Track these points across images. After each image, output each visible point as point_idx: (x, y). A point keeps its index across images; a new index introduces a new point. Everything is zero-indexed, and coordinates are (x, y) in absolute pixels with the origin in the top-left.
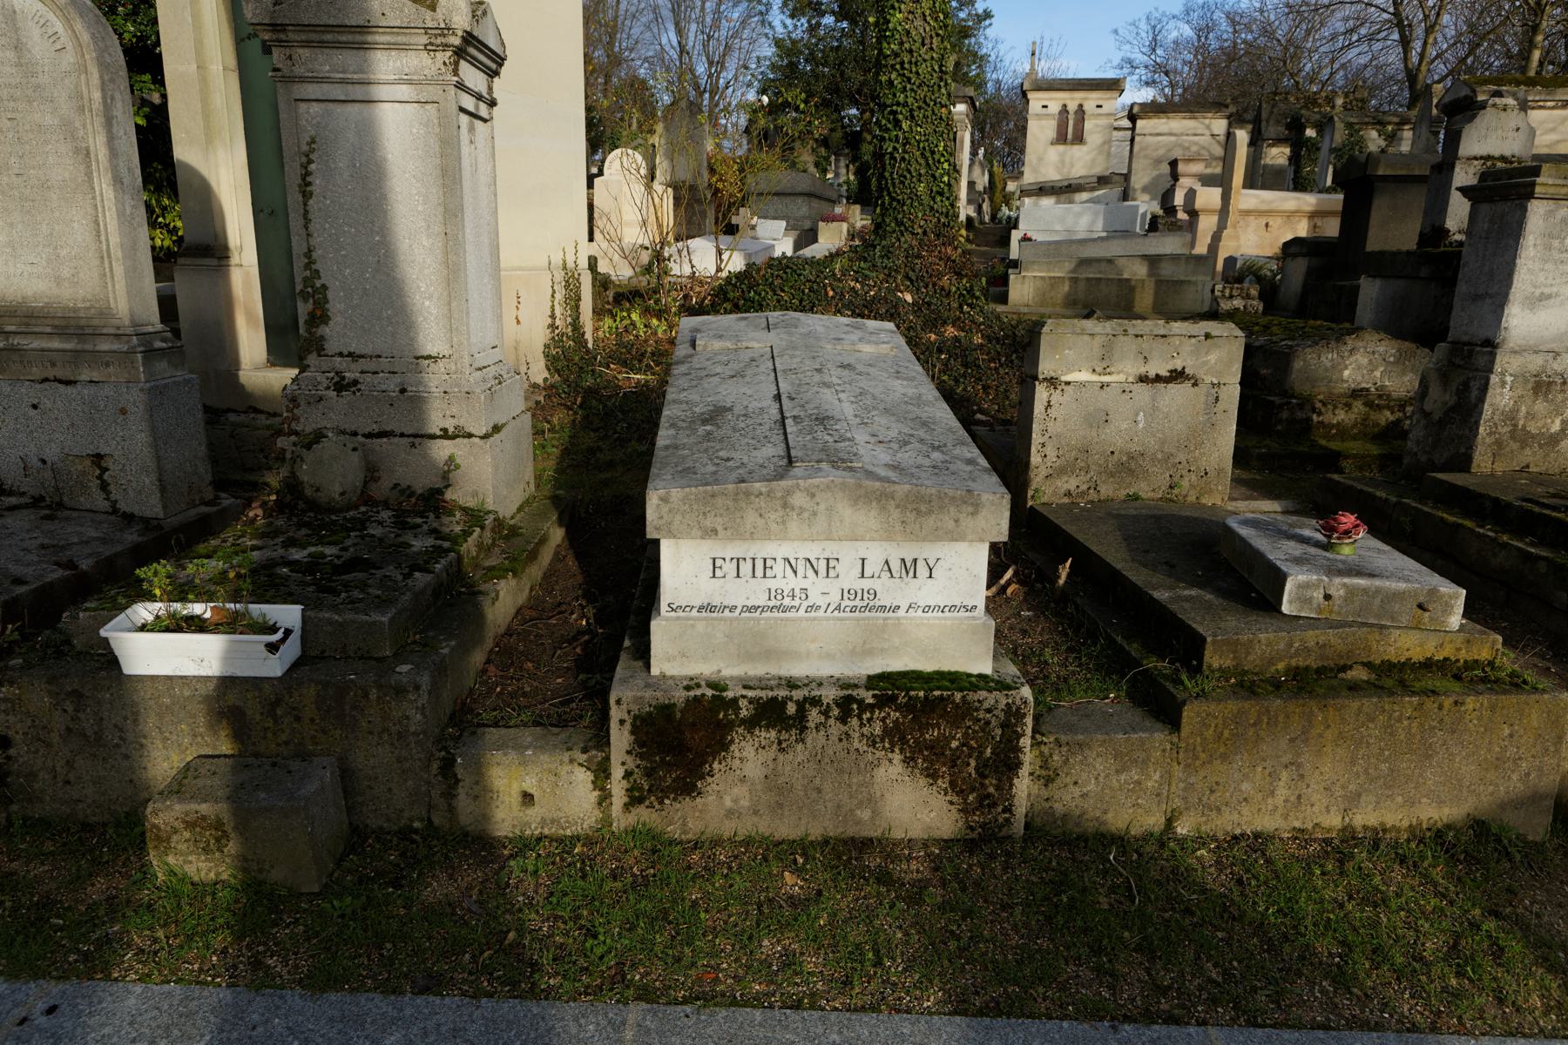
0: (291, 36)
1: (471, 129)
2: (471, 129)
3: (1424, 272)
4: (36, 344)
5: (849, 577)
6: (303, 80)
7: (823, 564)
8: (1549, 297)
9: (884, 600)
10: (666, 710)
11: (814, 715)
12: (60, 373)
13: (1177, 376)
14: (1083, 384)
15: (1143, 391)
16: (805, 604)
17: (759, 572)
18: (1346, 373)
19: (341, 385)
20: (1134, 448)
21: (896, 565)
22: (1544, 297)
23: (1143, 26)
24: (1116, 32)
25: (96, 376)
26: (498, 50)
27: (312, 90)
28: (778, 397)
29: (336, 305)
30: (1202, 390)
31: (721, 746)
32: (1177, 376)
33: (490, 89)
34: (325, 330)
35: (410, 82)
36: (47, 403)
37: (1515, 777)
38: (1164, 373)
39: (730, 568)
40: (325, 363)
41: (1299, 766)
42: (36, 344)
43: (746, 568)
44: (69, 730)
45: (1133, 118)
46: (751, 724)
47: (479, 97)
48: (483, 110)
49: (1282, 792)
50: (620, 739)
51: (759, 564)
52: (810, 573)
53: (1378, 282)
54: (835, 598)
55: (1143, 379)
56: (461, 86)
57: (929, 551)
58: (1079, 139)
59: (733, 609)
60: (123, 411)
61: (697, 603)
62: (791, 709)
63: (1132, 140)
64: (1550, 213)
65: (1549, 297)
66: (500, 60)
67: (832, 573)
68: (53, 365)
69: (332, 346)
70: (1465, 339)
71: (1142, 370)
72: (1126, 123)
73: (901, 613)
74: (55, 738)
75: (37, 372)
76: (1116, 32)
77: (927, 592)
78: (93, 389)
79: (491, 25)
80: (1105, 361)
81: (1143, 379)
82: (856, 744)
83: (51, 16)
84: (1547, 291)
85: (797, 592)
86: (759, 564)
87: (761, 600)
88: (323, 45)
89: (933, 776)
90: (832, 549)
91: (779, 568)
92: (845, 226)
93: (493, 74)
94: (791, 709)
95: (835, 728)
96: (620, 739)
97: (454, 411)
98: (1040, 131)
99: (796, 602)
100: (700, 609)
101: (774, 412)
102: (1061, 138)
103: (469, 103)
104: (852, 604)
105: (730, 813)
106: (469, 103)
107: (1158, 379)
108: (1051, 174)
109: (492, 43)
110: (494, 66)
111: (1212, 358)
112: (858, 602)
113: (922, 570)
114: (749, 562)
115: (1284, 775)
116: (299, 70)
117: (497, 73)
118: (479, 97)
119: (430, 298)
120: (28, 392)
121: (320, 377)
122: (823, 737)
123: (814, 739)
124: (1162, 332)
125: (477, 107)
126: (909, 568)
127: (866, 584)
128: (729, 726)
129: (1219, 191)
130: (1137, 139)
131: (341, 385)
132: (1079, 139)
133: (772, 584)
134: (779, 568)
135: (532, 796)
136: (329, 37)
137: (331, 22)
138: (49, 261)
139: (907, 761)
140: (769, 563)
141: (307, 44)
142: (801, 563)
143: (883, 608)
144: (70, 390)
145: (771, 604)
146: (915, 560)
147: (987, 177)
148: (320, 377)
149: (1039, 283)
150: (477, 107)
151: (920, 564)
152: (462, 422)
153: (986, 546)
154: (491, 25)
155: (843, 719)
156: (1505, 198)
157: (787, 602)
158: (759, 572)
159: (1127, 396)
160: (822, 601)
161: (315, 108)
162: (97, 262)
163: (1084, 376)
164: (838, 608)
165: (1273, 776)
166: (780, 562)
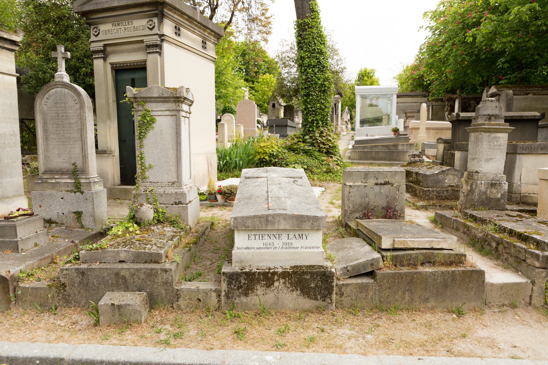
0: (139, 100)
1: (184, 120)
2: (184, 120)
7: (278, 236)
8: (492, 159)
13: (386, 183)
14: (359, 186)
15: (377, 188)
17: (261, 238)
18: (446, 181)
20: (376, 204)
21: (297, 236)
22: (491, 159)
28: (267, 192)
32: (386, 183)
35: (169, 110)
36: (65, 197)
37: (472, 293)
38: (383, 182)
39: (253, 237)
41: (411, 290)
42: (64, 181)
43: (257, 237)
44: (80, 282)
47: (186, 112)
48: (188, 115)
49: (407, 298)
51: (261, 236)
52: (274, 238)
53: (460, 152)
54: (281, 245)
55: (377, 184)
60: (86, 199)
64: (489, 136)
65: (492, 159)
66: (192, 102)
70: (471, 171)
71: (376, 182)
73: (299, 248)
74: (76, 285)
81: (377, 184)
82: (288, 285)
83: (74, 95)
84: (491, 157)
86: (261, 236)
87: (262, 246)
92: (356, 87)
93: (190, 105)
97: (178, 197)
99: (271, 246)
100: (245, 248)
101: (266, 195)
107: (381, 184)
112: (287, 246)
113: (304, 237)
115: (407, 293)
118: (186, 112)
123: (276, 284)
127: (289, 241)
136: (148, 100)
137: (150, 96)
138: (69, 158)
143: (294, 248)
147: (349, 116)
149: (360, 153)
151: (304, 235)
152: (181, 200)
156: (477, 132)
157: (268, 246)
158: (261, 238)
159: (372, 189)
160: (278, 246)
162: (82, 158)
163: (359, 184)
164: (282, 248)
165: (404, 293)
166: (266, 235)
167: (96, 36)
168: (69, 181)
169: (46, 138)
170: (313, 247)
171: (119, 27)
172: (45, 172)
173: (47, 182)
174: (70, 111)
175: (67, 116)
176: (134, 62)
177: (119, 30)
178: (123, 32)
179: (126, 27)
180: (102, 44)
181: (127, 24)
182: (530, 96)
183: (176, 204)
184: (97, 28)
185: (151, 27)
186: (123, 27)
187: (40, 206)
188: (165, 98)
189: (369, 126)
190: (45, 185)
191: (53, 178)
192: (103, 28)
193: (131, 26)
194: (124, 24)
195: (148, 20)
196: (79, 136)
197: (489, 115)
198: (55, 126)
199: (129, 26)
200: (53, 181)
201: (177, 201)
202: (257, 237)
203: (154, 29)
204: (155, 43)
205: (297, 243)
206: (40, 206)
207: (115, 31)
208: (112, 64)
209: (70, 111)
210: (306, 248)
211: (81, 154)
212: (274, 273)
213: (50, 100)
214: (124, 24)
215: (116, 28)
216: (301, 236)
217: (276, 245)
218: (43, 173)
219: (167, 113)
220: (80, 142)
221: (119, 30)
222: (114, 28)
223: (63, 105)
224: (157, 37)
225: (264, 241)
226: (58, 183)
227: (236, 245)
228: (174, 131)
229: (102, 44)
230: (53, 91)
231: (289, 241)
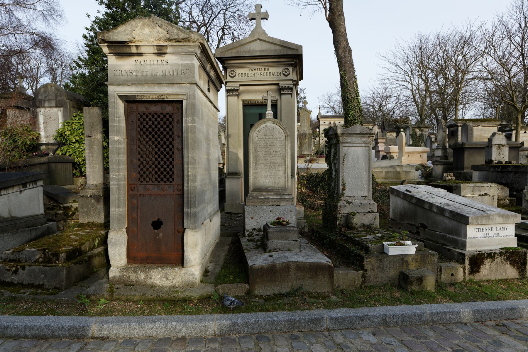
3: (492, 170)
4: (271, 197)
5: (495, 231)
6: (345, 143)
10: (474, 256)
11: (496, 256)
12: (276, 203)
13: (486, 194)
15: (480, 197)
19: (349, 203)
23: (326, 96)
24: (318, 98)
25: (284, 204)
27: (346, 145)
29: (347, 187)
30: (491, 197)
31: (482, 263)
32: (486, 194)
34: (344, 192)
39: (477, 230)
40: (344, 199)
46: (487, 258)
50: (467, 262)
53: (478, 172)
54: (493, 235)
55: (480, 195)
57: (506, 226)
60: (291, 211)
62: (493, 254)
68: (275, 201)
69: (345, 195)
74: (375, 269)
75: (271, 204)
76: (318, 98)
77: (506, 233)
78: (283, 207)
80: (473, 192)
81: (480, 195)
87: (482, 236)
88: (350, 136)
89: (514, 266)
90: (492, 226)
94: (493, 254)
95: (499, 258)
96: (467, 262)
105: (484, 275)
107: (483, 195)
111: (492, 190)
116: (344, 141)
120: (270, 208)
121: (344, 202)
122: (498, 260)
123: (496, 260)
126: (503, 228)
127: (497, 232)
128: (483, 259)
129: (466, 155)
131: (349, 203)
133: (484, 233)
134: (484, 229)
139: (510, 263)
141: (347, 136)
144: (280, 207)
148: (344, 202)
153: (514, 226)
155: (500, 256)
161: (346, 148)
163: (469, 195)
167: (232, 77)
168: (275, 197)
169: (256, 163)
171: (255, 72)
172: (254, 190)
173: (257, 198)
174: (277, 142)
175: (274, 146)
176: (251, 101)
177: (256, 74)
178: (259, 76)
179: (263, 72)
180: (238, 84)
181: (263, 70)
182: (480, 127)
184: (233, 71)
185: (286, 74)
186: (259, 72)
187: (252, 218)
188: (364, 134)
190: (256, 200)
191: (262, 195)
192: (239, 71)
193: (267, 72)
194: (261, 69)
195: (284, 68)
196: (283, 161)
197: (498, 145)
198: (264, 153)
199: (265, 72)
200: (262, 197)
201: (370, 210)
203: (289, 76)
204: (289, 86)
206: (252, 218)
207: (251, 75)
208: (244, 101)
209: (277, 142)
211: (284, 176)
212: (495, 253)
213: (261, 133)
214: (261, 69)
215: (252, 72)
218: (252, 191)
219: (363, 145)
220: (284, 167)
221: (256, 74)
222: (250, 72)
223: (271, 137)
224: (291, 82)
225: (484, 233)
226: (267, 199)
227: (468, 236)
229: (238, 84)
230: (264, 125)
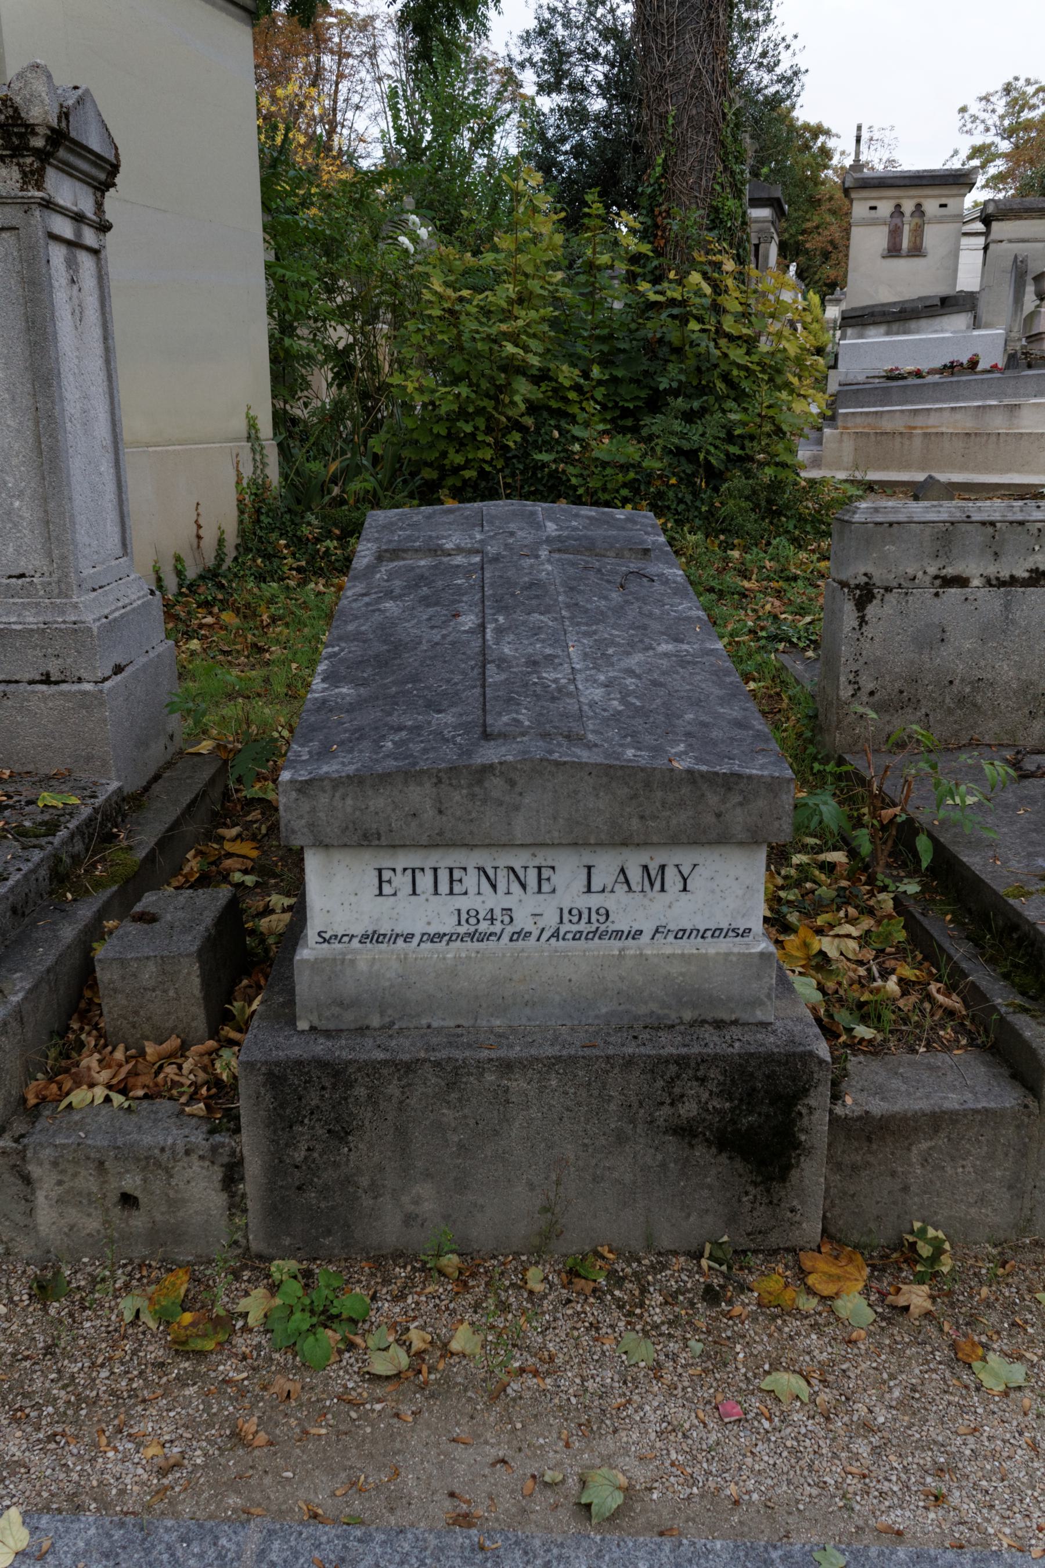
1: (71, 264)
9: (621, 922)
16: (509, 930)
17: (444, 887)
21: (635, 875)
26: (110, 156)
33: (99, 206)
38: (1022, 573)
39: (403, 882)
43: (425, 881)
45: (987, 220)
47: (78, 218)
48: (89, 237)
52: (515, 887)
54: (550, 920)
56: (48, 205)
58: (917, 251)
59: (408, 937)
61: (358, 930)
63: (986, 248)
67: (546, 887)
72: (979, 226)
73: (645, 938)
79: (91, 114)
85: (497, 913)
87: (448, 925)
91: (471, 880)
93: (102, 187)
98: (866, 243)
99: (497, 928)
100: (365, 938)
102: (893, 251)
103: (64, 228)
104: (575, 928)
106: (64, 228)
107: (1013, 581)
108: (886, 295)
109: (95, 143)
110: (102, 176)
112: (582, 926)
114: (429, 874)
117: (109, 185)
119: (21, 495)
124: (1019, 517)
125: (78, 233)
127: (594, 901)
130: (992, 246)
132: (917, 251)
133: (464, 903)
134: (471, 880)
135: (136, 1199)
140: (457, 874)
142: (502, 874)
143: (618, 934)
145: (462, 930)
146: (662, 868)
150: (78, 233)
151: (671, 873)
154: (91, 114)
157: (484, 926)
158: (444, 887)
164: (556, 935)
166: (472, 873)
170: (717, 932)
183: (47, 680)
189: (888, 333)
202: (425, 881)
205: (630, 911)
210: (681, 934)
216: (654, 879)
217: (523, 921)
228: (128, 535)
231: (594, 901)
